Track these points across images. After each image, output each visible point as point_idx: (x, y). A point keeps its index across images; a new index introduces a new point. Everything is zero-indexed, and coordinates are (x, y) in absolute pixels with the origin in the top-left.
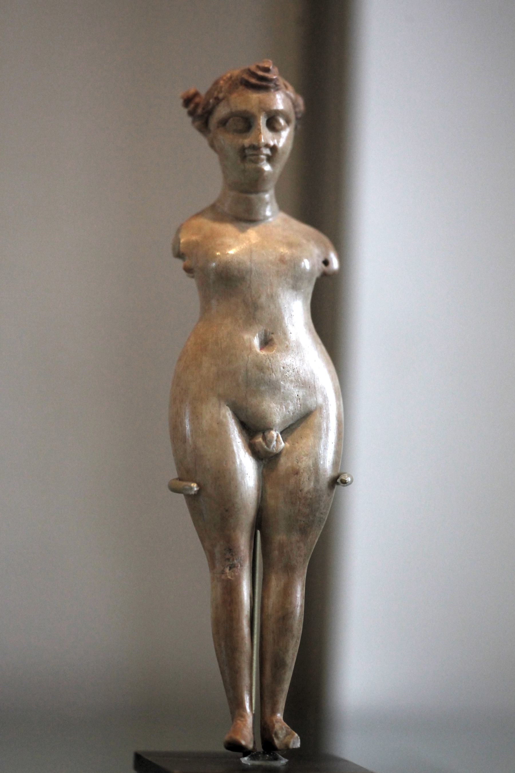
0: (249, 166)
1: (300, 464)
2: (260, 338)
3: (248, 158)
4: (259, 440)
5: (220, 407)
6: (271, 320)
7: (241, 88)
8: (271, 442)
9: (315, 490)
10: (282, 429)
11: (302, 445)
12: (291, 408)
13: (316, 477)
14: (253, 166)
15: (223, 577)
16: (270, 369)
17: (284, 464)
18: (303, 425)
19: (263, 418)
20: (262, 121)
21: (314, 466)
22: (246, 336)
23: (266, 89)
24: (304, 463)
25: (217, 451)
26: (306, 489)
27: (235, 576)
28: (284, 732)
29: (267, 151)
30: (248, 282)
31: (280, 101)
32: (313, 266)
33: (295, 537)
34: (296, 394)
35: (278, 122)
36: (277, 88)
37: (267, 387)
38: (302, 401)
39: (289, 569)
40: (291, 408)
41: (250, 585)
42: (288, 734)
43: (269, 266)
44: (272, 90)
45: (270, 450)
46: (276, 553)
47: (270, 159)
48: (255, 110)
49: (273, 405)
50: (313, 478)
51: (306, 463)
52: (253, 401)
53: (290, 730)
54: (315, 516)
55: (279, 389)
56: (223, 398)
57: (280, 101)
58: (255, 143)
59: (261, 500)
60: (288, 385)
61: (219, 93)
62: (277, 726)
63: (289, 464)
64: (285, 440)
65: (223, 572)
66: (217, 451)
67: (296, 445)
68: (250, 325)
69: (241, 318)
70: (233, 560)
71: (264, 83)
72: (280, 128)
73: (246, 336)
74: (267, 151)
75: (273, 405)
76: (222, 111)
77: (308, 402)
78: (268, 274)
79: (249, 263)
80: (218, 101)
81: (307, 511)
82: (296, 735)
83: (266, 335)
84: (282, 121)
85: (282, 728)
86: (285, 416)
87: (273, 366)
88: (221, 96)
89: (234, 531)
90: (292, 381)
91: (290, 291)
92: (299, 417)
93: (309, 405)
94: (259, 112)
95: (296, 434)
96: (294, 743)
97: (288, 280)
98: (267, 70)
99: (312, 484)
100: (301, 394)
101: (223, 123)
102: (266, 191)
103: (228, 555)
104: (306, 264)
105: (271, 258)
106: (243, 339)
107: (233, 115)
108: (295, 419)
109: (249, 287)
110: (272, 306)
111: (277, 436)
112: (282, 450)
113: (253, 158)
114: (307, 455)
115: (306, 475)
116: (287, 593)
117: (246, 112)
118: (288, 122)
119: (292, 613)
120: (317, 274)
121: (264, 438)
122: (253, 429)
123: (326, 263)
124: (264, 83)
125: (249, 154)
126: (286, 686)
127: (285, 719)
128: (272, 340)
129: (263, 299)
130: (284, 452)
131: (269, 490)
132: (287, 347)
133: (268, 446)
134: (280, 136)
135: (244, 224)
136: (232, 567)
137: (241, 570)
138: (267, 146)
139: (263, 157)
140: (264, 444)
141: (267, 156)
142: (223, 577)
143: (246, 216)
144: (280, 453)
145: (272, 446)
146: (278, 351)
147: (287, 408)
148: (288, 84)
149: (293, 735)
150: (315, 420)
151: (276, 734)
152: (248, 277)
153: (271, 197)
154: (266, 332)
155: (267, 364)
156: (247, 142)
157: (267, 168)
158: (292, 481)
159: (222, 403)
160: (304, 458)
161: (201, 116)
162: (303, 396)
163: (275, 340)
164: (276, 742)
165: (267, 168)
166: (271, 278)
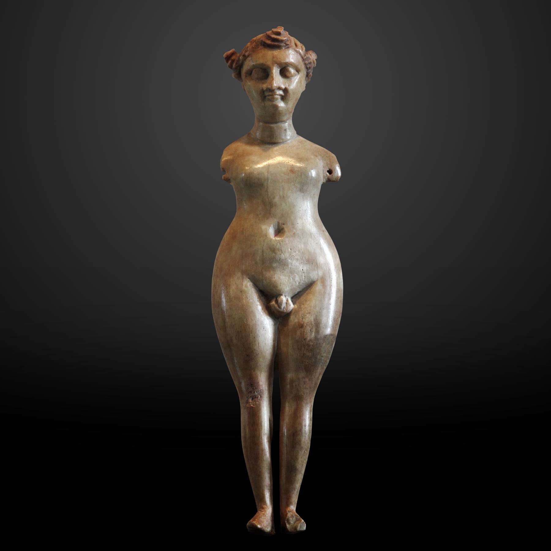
0: (268, 103)
1: (304, 320)
2: (274, 228)
3: (267, 97)
4: (273, 303)
5: (243, 279)
6: (282, 215)
7: (261, 47)
8: (281, 304)
9: (316, 338)
10: (292, 295)
11: (306, 306)
12: (297, 278)
13: (316, 329)
14: (270, 103)
15: (248, 405)
16: (280, 250)
17: (293, 320)
18: (308, 291)
19: (275, 286)
20: (276, 71)
21: (315, 321)
22: (264, 227)
23: (279, 47)
24: (307, 319)
25: (239, 311)
26: (309, 338)
27: (256, 404)
28: (294, 518)
29: (281, 92)
30: (266, 187)
31: (292, 56)
32: (318, 174)
33: (302, 374)
34: (301, 268)
35: (288, 71)
36: (288, 47)
37: (277, 264)
38: (306, 274)
39: (299, 399)
40: (297, 278)
41: (270, 411)
42: (297, 520)
43: (282, 175)
44: (284, 48)
45: (282, 310)
46: (288, 386)
47: (283, 98)
48: (269, 63)
49: (282, 277)
50: (314, 330)
51: (309, 319)
52: (268, 274)
53: (299, 517)
54: (316, 358)
55: (288, 266)
56: (246, 273)
57: (292, 56)
58: (270, 87)
59: (277, 349)
60: (294, 262)
61: (246, 51)
62: (289, 515)
63: (296, 321)
64: (294, 304)
65: (247, 402)
66: (239, 311)
67: (302, 306)
68: (267, 218)
69: (260, 214)
70: (254, 392)
71: (276, 43)
72: (290, 75)
73: (264, 227)
74: (281, 92)
75: (282, 277)
76: (248, 64)
77: (311, 275)
78: (281, 181)
79: (266, 174)
80: (245, 57)
81: (310, 354)
82: (303, 521)
83: (278, 226)
84: (292, 71)
85: (292, 516)
86: (292, 285)
87: (283, 249)
88: (247, 54)
89: (254, 371)
90: (297, 259)
91: (298, 193)
92: (304, 286)
93: (312, 277)
94: (273, 64)
95: (302, 298)
96: (301, 527)
97: (296, 185)
98: (279, 34)
99: (313, 334)
100: (305, 269)
101: (249, 73)
102: (284, 122)
103: (250, 389)
104: (313, 173)
105: (283, 169)
106: (261, 229)
107: (254, 67)
108: (302, 288)
109: (267, 191)
110: (284, 204)
111: (287, 300)
112: (292, 310)
113: (270, 97)
114: (310, 313)
115: (308, 328)
116: (297, 416)
117: (262, 64)
118: (298, 71)
119: (301, 430)
120: (322, 180)
121: (277, 302)
122: (269, 296)
123: (330, 172)
124: (276, 43)
125: (267, 94)
126: (298, 485)
127: (297, 511)
128: (283, 229)
129: (277, 200)
130: (293, 311)
131: (282, 341)
132: (294, 234)
133: (280, 307)
134: (291, 82)
135: (267, 146)
136: (254, 398)
137: (261, 400)
138: (279, 88)
139: (276, 96)
140: (276, 305)
141: (281, 95)
142: (248, 405)
143: (269, 140)
144: (291, 312)
145: (282, 307)
146: (287, 237)
147: (294, 279)
148: (298, 43)
149: (301, 521)
150: (318, 287)
151: (288, 520)
152: (265, 184)
153: (289, 125)
154: (278, 223)
155: (278, 247)
156: (265, 86)
157: (281, 104)
158: (298, 333)
159: (245, 276)
160: (308, 315)
161: (236, 68)
162: (307, 270)
163: (286, 229)
164: (288, 526)
165: (281, 104)
166: (283, 184)
